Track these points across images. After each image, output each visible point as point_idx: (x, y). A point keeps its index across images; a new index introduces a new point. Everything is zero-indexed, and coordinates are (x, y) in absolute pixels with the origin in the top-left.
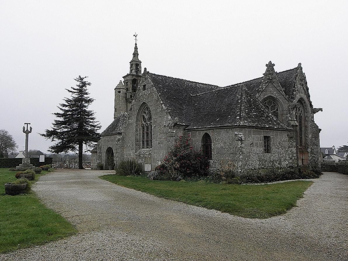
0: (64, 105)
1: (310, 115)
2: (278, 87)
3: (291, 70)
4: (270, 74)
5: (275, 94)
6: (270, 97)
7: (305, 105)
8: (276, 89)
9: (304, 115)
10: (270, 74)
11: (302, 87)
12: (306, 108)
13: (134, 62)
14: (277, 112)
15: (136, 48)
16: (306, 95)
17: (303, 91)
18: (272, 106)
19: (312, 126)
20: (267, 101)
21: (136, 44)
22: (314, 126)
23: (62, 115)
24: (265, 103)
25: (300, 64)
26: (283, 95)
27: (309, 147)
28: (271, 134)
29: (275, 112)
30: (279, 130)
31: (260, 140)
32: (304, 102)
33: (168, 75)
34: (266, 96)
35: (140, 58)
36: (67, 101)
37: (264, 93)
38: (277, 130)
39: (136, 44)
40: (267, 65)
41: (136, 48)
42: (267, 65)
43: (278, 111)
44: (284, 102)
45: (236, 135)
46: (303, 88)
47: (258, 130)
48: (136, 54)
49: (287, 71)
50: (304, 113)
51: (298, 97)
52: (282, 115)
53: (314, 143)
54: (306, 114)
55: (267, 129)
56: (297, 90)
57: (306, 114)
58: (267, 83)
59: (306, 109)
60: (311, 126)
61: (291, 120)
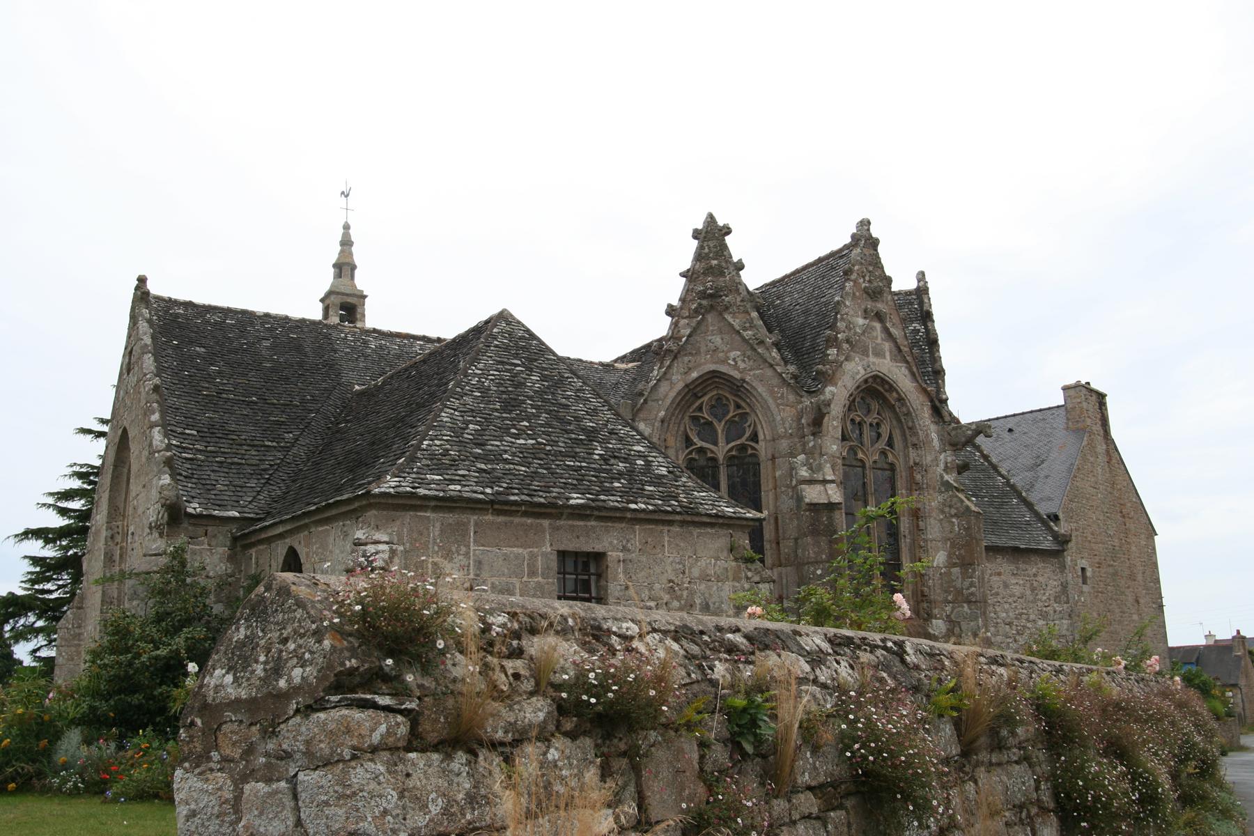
0: (68, 495)
1: (936, 459)
2: (745, 329)
3: (832, 254)
4: (709, 271)
5: (735, 363)
6: (714, 378)
7: (904, 409)
8: (737, 338)
9: (906, 456)
10: (709, 271)
11: (878, 325)
12: (910, 424)
13: (332, 298)
14: (753, 448)
15: (346, 243)
16: (907, 362)
17: (887, 346)
18: (731, 421)
19: (947, 509)
20: (706, 398)
21: (347, 227)
22: (953, 511)
23: (61, 533)
24: (700, 409)
25: (865, 224)
26: (771, 366)
27: (936, 611)
28: (608, 541)
29: (743, 448)
30: (670, 523)
31: (532, 573)
32: (894, 394)
33: (259, 306)
34: (695, 375)
35: (362, 281)
36: (80, 476)
37: (686, 359)
38: (639, 519)
39: (347, 227)
40: (696, 234)
41: (346, 243)
42: (696, 234)
43: (757, 442)
44: (775, 399)
45: (358, 543)
46: (886, 330)
47: (517, 520)
48: (344, 267)
49: (820, 260)
50: (906, 447)
51: (854, 371)
52: (773, 458)
53: (959, 592)
54: (913, 454)
55: (579, 513)
56: (848, 341)
57: (913, 454)
58: (696, 311)
59: (910, 428)
60: (943, 512)
61: (811, 482)
